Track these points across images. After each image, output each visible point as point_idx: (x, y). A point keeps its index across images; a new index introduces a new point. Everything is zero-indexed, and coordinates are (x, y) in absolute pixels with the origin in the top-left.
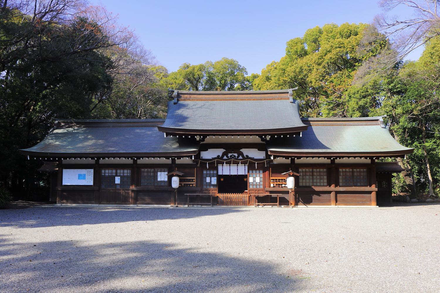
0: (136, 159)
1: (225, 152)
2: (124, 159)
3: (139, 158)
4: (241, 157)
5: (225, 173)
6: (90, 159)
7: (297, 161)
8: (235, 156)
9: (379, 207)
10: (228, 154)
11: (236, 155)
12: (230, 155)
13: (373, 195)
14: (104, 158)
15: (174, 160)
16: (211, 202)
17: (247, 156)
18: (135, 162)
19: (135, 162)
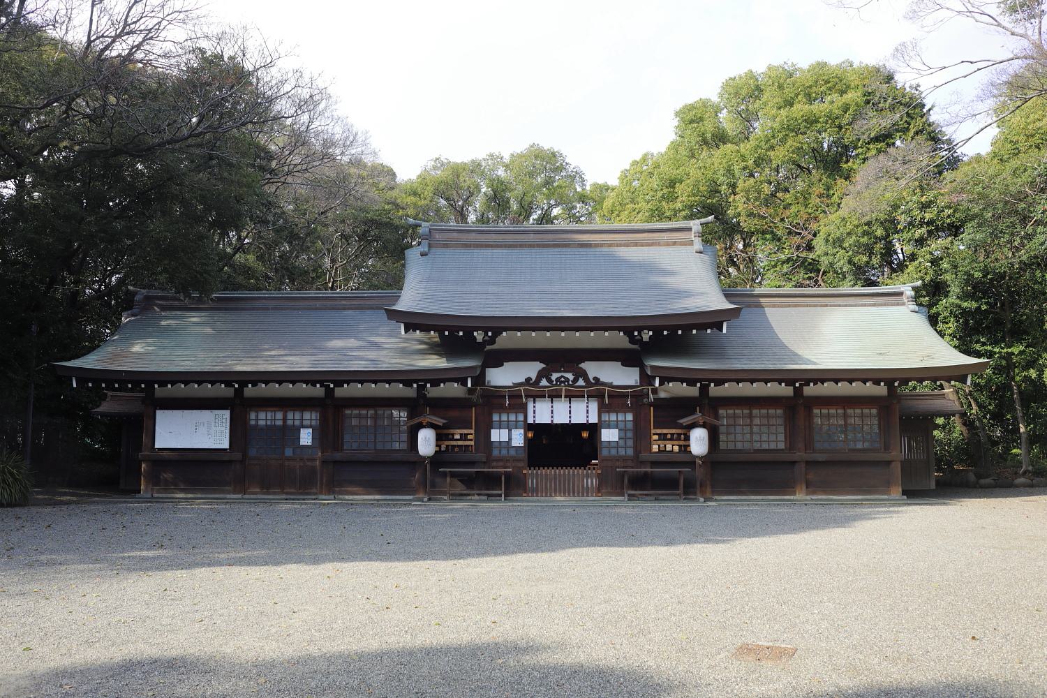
0: (332, 386)
3: (339, 384)
4: (581, 382)
6: (223, 386)
8: (567, 380)
11: (570, 376)
12: (555, 376)
13: (897, 468)
17: (596, 379)
18: (329, 392)
19: (329, 392)
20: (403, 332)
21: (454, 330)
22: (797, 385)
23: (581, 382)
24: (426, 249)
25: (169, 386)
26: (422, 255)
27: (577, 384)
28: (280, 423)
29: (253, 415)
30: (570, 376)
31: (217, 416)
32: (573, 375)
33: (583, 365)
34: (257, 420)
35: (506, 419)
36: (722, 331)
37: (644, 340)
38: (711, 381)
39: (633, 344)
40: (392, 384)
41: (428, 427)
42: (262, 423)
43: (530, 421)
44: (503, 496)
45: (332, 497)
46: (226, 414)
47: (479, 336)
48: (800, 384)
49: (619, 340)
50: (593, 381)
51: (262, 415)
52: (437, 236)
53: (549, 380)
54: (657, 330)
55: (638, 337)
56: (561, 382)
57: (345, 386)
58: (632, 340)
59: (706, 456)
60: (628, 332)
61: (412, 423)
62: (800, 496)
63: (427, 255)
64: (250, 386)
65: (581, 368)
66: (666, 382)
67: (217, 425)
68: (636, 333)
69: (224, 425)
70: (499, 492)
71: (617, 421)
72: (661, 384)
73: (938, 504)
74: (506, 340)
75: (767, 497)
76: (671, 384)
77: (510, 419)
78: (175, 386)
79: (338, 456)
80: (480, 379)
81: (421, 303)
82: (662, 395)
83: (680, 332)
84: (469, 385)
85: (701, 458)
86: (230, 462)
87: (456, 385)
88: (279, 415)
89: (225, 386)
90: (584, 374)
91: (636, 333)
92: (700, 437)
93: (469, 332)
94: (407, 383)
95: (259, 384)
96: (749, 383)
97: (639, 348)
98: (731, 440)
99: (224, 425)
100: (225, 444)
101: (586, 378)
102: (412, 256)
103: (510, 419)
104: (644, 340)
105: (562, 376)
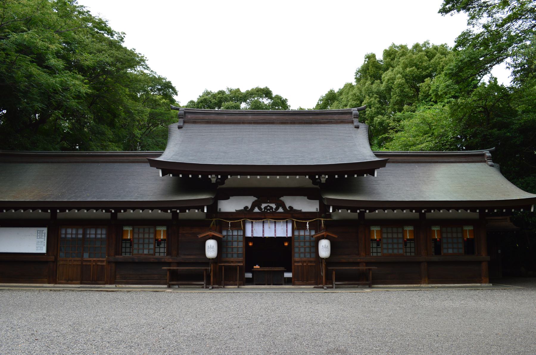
0: (178, 211)
1: (256, 201)
4: (281, 210)
6: (40, 211)
8: (272, 208)
9: (493, 285)
10: (261, 205)
11: (274, 206)
12: (263, 206)
13: (484, 266)
14: (63, 210)
17: (291, 208)
18: (175, 214)
19: (422, 216)
20: (161, 175)
21: (186, 174)
22: (423, 211)
23: (281, 210)
24: (182, 124)
25: (67, 211)
26: (355, 127)
27: (278, 211)
28: (80, 236)
29: (63, 231)
30: (274, 206)
31: (39, 232)
32: (276, 205)
33: (282, 199)
34: (66, 234)
36: (374, 176)
37: (322, 182)
38: (366, 209)
39: (314, 185)
40: (191, 210)
41: (212, 239)
42: (69, 236)
43: (249, 234)
44: (205, 285)
45: (114, 286)
46: (45, 230)
47: (213, 178)
48: (425, 211)
49: (305, 181)
51: (69, 231)
52: (189, 116)
53: (260, 208)
54: (331, 175)
55: (318, 180)
56: (268, 210)
57: (187, 211)
58: (315, 181)
59: (329, 258)
60: (312, 177)
61: (318, 235)
63: (182, 128)
64: (122, 211)
65: (281, 201)
66: (337, 210)
67: (38, 237)
68: (317, 177)
69: (43, 237)
70: (203, 283)
72: (333, 211)
74: (231, 181)
76: (340, 211)
77: (234, 234)
78: (26, 211)
79: (119, 258)
80: (213, 207)
81: (174, 156)
82: (335, 218)
83: (346, 176)
84: (205, 211)
85: (326, 259)
86: (47, 262)
87: (196, 211)
88: (81, 231)
89: (106, 212)
90: (283, 205)
91: (317, 177)
92: (325, 246)
93: (205, 175)
94: (164, 210)
95: (128, 210)
96: (382, 210)
97: (319, 188)
98: (162, 253)
99: (43, 237)
100: (44, 250)
102: (173, 128)
103: (234, 234)
104: (322, 182)
105: (268, 206)
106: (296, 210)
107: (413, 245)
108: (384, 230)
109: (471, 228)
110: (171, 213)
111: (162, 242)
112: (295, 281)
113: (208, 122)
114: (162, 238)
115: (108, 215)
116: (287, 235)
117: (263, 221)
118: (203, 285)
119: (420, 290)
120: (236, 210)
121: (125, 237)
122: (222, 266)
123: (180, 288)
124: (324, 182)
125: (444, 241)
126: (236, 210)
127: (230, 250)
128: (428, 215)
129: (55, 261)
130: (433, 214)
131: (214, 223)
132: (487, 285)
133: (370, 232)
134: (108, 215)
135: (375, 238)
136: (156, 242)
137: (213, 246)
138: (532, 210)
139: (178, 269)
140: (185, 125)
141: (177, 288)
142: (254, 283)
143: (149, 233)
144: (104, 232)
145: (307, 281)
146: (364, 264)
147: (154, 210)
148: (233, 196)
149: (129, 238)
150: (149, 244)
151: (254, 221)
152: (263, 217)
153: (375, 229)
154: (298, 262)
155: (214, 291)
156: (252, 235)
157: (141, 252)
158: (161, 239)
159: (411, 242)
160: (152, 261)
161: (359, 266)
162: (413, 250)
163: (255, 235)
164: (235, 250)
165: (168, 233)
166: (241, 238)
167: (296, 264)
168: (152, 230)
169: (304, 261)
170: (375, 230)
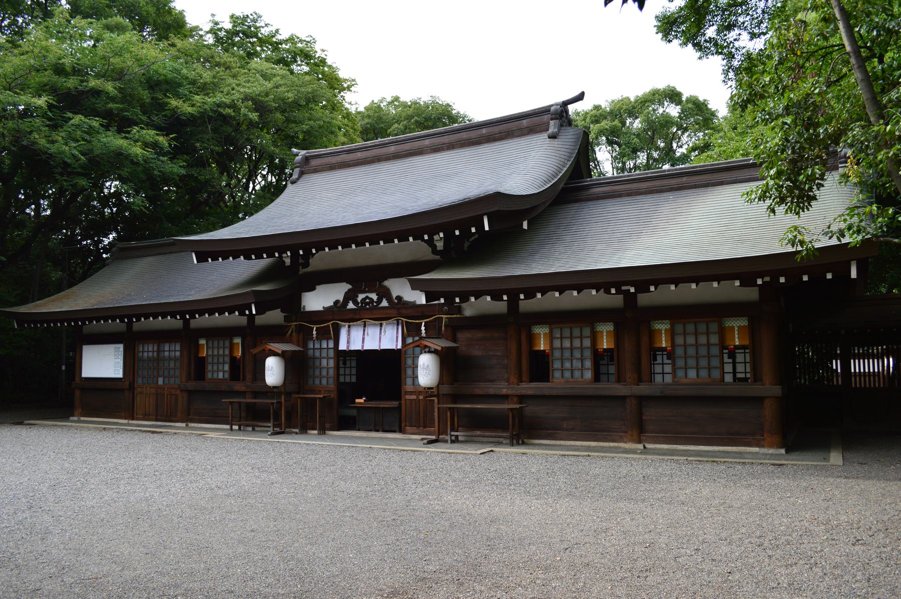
0: (632, 290)
1: (349, 290)
2: (594, 292)
3: (642, 287)
4: (385, 303)
5: (353, 347)
6: (489, 298)
7: (526, 305)
8: (371, 299)
9: (787, 452)
10: (358, 296)
11: (374, 296)
12: (361, 297)
13: (769, 410)
14: (530, 295)
15: (513, 302)
16: (272, 421)
17: (399, 298)
18: (630, 299)
19: (630, 299)
23: (385, 303)
25: (539, 295)
26: (550, 137)
35: (319, 347)
40: (722, 282)
43: (343, 346)
44: (272, 428)
50: (396, 301)
62: (836, 458)
70: (270, 425)
71: (164, 351)
73: (44, 426)
75: (622, 445)
90: (385, 293)
101: (390, 299)
105: (367, 297)
106: (407, 303)
107: (354, 364)
108: (679, 328)
109: (743, 322)
110: (182, 321)
111: (737, 351)
112: (406, 426)
113: (332, 167)
114: (605, 347)
115: (243, 321)
116: (363, 346)
117: (365, 322)
118: (270, 427)
119: (589, 456)
120: (323, 307)
121: (657, 345)
122: (316, 398)
123: (257, 431)
124: (442, 248)
125: (557, 354)
126: (323, 307)
127: (317, 372)
128: (643, 299)
129: (132, 387)
130: (655, 296)
131: (293, 329)
132: (771, 451)
133: (652, 335)
134: (243, 321)
135: (664, 346)
136: (725, 351)
137: (272, 367)
138: (854, 274)
139: (255, 403)
140: (305, 177)
141: (782, 455)
142: (357, 428)
143: (708, 334)
144: (178, 347)
145: (425, 427)
146: (515, 399)
147: (680, 284)
148: (319, 284)
149: (542, 349)
150: (224, 363)
151: (384, 323)
152: (358, 317)
153: (541, 331)
154: (411, 393)
155: (456, 449)
156: (348, 347)
157: (215, 375)
158: (604, 349)
159: (352, 358)
160: (223, 389)
161: (245, 398)
162: (354, 371)
163: (352, 348)
164: (324, 373)
165: (618, 336)
166: (331, 353)
167: (408, 397)
168: (714, 327)
169: (420, 392)
170: (605, 331)
